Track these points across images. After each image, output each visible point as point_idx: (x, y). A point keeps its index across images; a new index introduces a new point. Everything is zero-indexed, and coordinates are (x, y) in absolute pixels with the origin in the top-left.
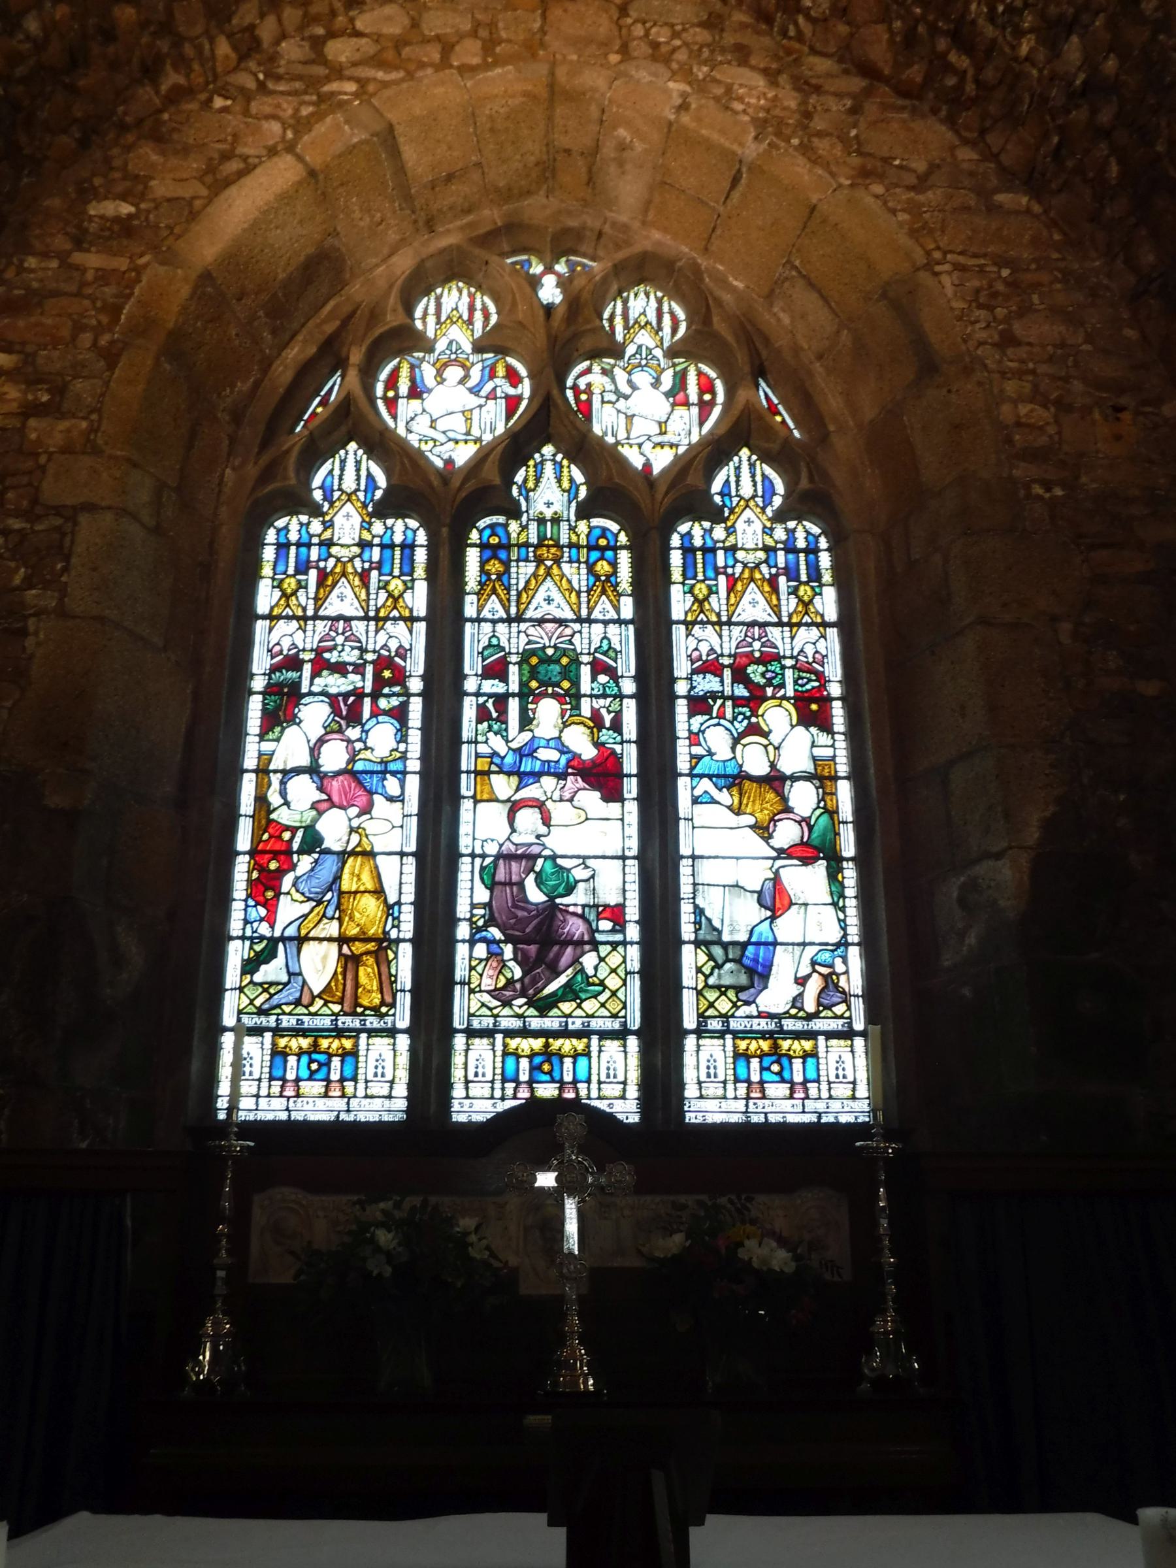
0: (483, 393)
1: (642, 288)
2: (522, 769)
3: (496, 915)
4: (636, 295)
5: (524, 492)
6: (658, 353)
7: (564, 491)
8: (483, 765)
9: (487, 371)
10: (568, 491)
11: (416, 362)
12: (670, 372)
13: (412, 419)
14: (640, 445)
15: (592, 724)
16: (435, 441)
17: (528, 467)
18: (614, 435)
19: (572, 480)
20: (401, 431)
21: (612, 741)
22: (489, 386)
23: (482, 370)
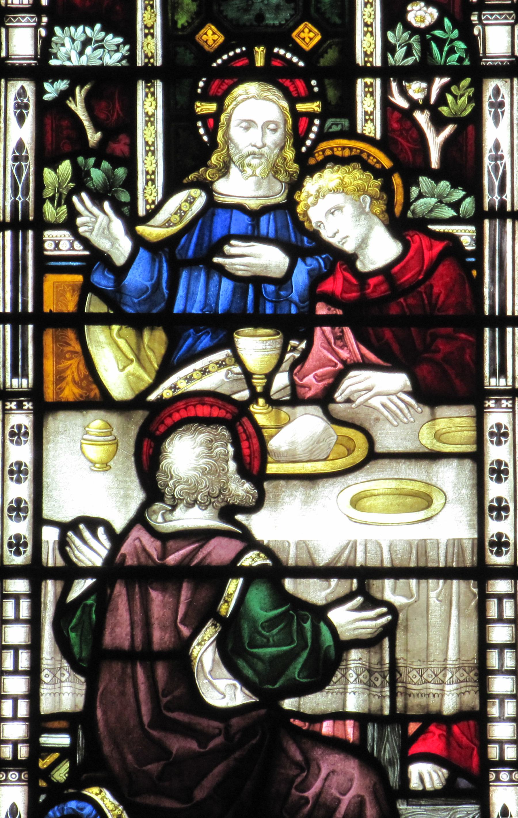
2: (178, 307)
3: (107, 749)
8: (60, 294)
15: (387, 163)
21: (450, 213)
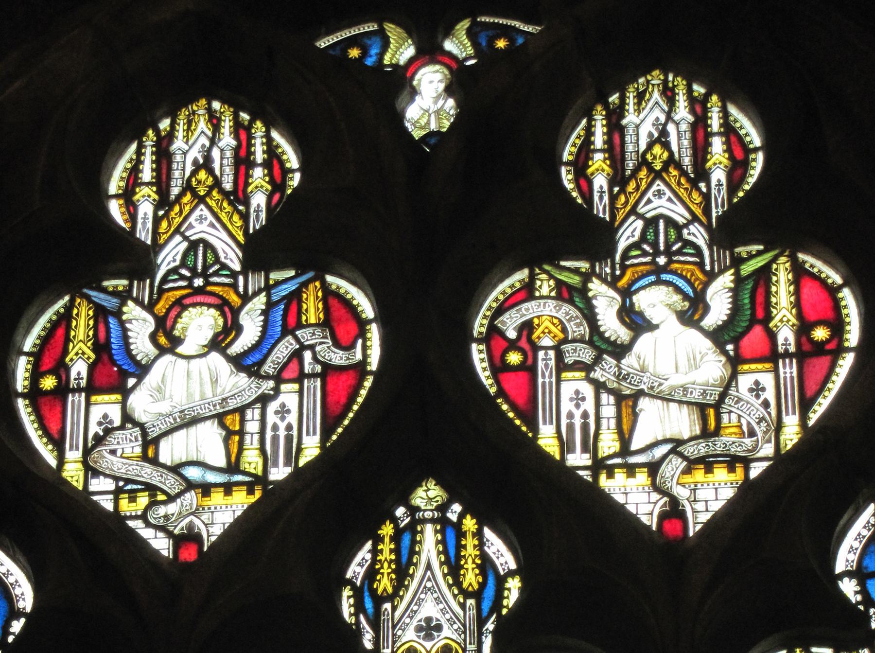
0: (268, 368)
1: (656, 77)
4: (641, 97)
5: (369, 604)
6: (698, 235)
7: (467, 594)
9: (278, 314)
10: (478, 595)
11: (110, 302)
12: (726, 279)
13: (99, 440)
14: (653, 468)
16: (151, 489)
17: (378, 540)
18: (590, 445)
19: (486, 564)
20: (73, 473)
22: (284, 349)
23: (265, 313)
